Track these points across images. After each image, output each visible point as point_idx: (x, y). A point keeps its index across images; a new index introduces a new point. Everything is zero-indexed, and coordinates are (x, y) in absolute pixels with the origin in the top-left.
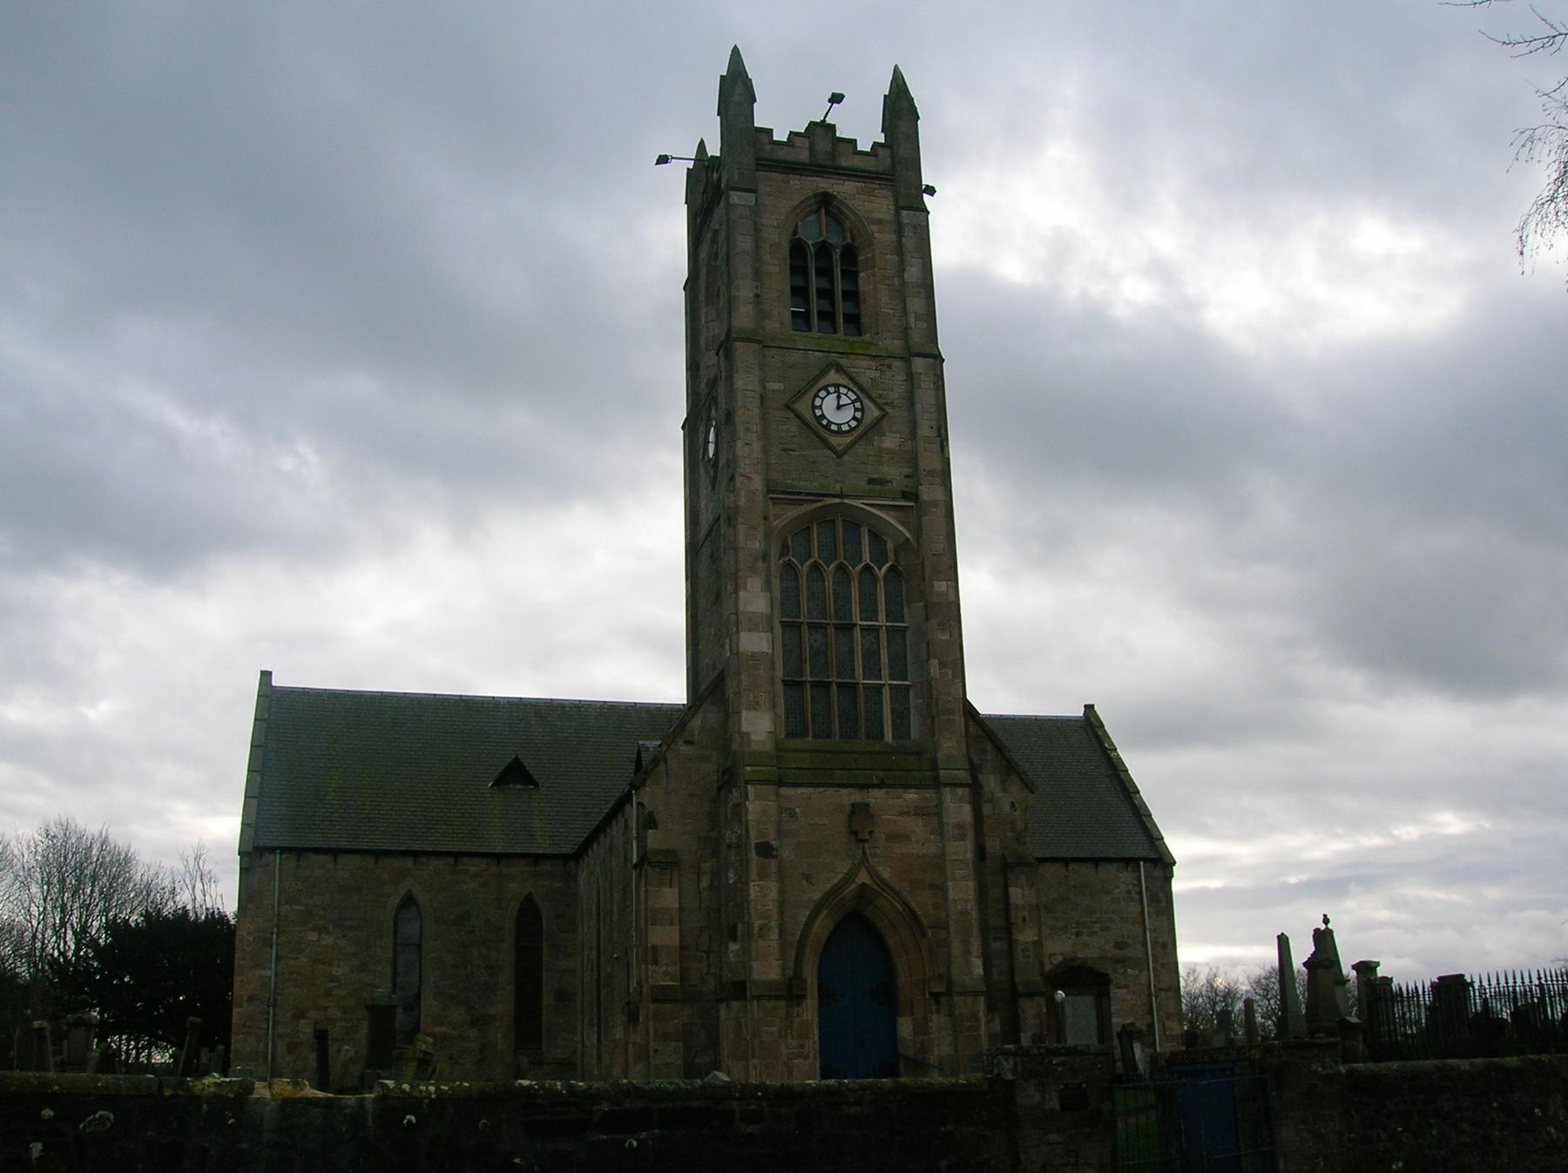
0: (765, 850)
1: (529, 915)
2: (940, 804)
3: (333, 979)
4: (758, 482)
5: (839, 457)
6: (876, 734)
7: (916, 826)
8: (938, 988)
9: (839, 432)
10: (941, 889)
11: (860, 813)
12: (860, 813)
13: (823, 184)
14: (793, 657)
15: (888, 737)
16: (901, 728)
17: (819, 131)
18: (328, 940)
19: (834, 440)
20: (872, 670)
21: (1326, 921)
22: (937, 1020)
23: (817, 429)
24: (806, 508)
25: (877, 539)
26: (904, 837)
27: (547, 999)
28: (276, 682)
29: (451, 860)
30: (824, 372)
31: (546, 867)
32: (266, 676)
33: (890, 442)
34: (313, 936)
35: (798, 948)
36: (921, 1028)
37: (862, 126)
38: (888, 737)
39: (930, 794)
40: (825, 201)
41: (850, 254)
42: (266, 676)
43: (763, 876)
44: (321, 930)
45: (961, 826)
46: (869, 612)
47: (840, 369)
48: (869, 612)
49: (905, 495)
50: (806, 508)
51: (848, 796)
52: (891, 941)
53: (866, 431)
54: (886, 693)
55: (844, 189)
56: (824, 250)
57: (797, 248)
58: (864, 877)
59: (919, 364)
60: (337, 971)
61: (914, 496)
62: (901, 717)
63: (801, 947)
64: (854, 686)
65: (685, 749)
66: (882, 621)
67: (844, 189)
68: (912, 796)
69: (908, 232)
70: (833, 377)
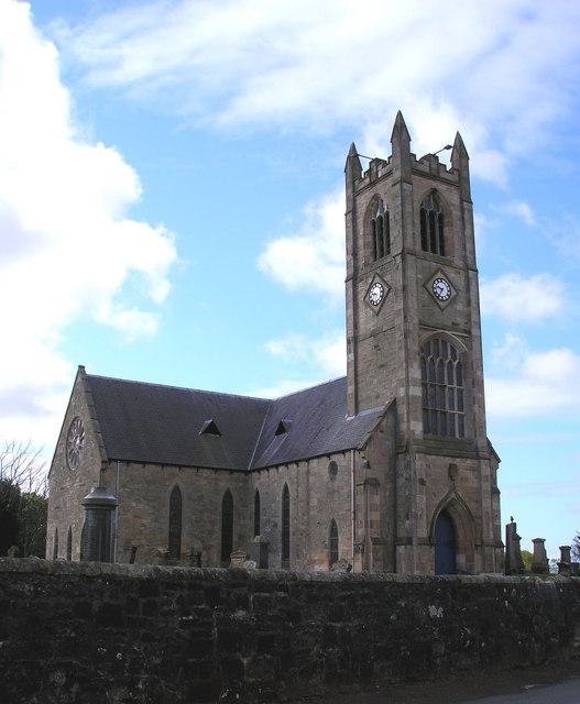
0: (422, 482)
1: (228, 495)
2: (479, 466)
3: (144, 525)
4: (416, 321)
5: (442, 310)
6: (453, 434)
7: (470, 475)
8: (479, 543)
9: (442, 300)
10: (479, 502)
11: (452, 467)
12: (452, 467)
13: (435, 184)
14: (425, 395)
15: (457, 436)
16: (462, 434)
17: (432, 159)
18: (141, 506)
19: (441, 304)
20: (452, 407)
21: (512, 520)
22: (477, 557)
23: (434, 297)
24: (431, 333)
25: (453, 350)
26: (466, 479)
27: (235, 538)
28: (89, 371)
29: (195, 470)
30: (436, 272)
31: (236, 475)
32: (82, 368)
33: (460, 307)
34: (134, 504)
35: (256, 514)
36: (470, 559)
37: (445, 159)
38: (457, 436)
39: (476, 462)
40: (434, 191)
41: (441, 217)
42: (82, 368)
43: (421, 493)
44: (137, 501)
45: (487, 476)
46: (451, 382)
47: (442, 271)
48: (451, 382)
49: (466, 332)
50: (431, 333)
51: (448, 460)
52: (457, 522)
53: (452, 300)
54: (456, 416)
55: (442, 187)
56: (432, 214)
57: (422, 212)
58: (453, 495)
59: (471, 273)
60: (144, 521)
61: (469, 332)
62: (462, 426)
63: (433, 523)
64: (444, 413)
65: (380, 434)
66: (455, 385)
67: (442, 187)
68: (469, 461)
69: (466, 212)
70: (439, 275)
